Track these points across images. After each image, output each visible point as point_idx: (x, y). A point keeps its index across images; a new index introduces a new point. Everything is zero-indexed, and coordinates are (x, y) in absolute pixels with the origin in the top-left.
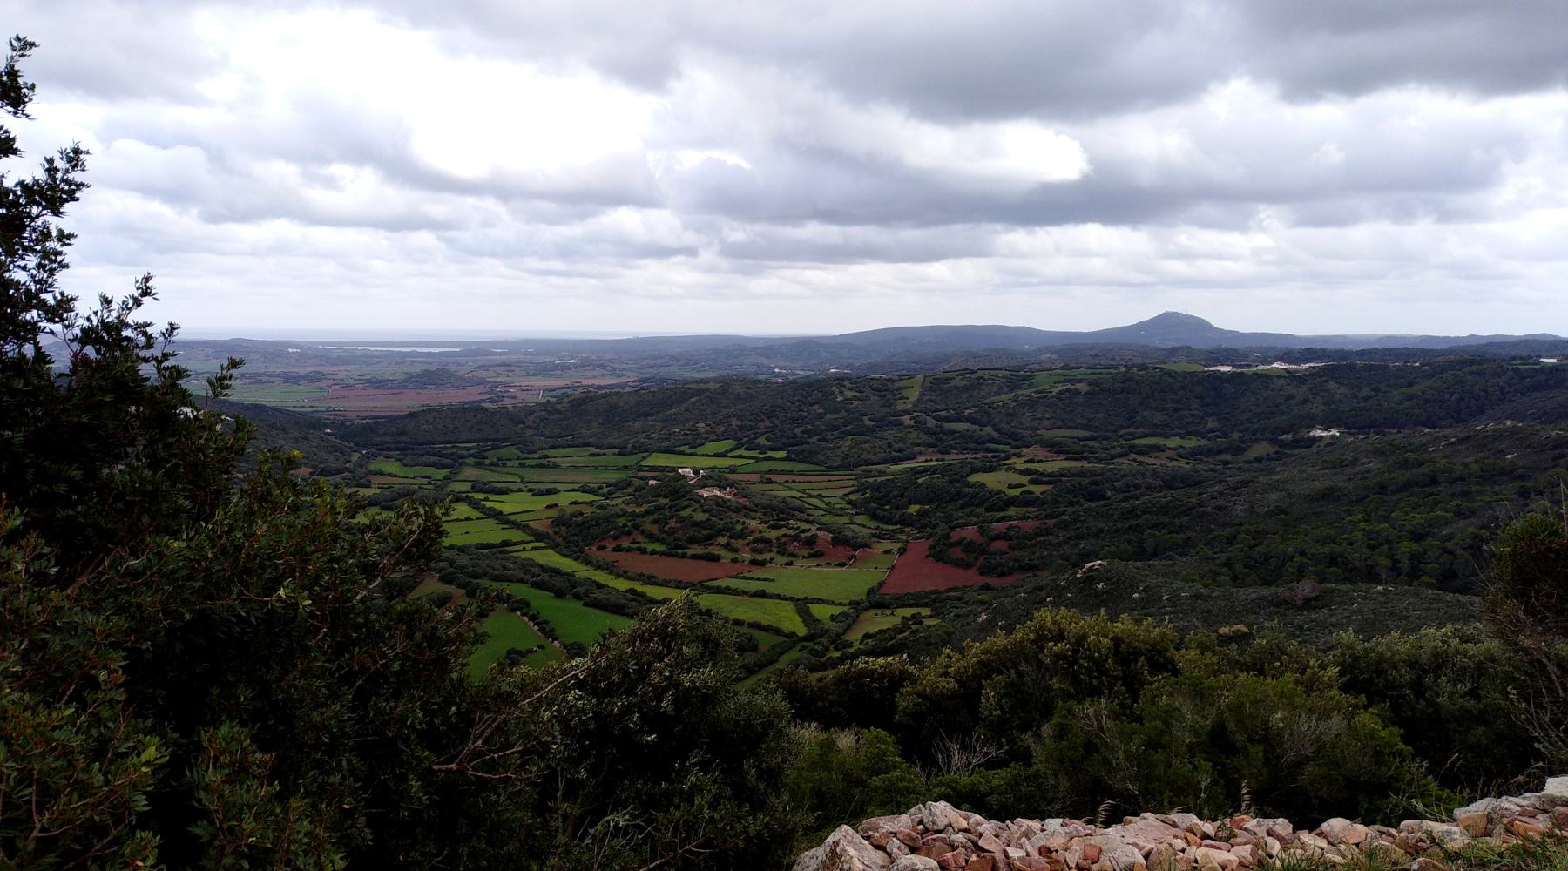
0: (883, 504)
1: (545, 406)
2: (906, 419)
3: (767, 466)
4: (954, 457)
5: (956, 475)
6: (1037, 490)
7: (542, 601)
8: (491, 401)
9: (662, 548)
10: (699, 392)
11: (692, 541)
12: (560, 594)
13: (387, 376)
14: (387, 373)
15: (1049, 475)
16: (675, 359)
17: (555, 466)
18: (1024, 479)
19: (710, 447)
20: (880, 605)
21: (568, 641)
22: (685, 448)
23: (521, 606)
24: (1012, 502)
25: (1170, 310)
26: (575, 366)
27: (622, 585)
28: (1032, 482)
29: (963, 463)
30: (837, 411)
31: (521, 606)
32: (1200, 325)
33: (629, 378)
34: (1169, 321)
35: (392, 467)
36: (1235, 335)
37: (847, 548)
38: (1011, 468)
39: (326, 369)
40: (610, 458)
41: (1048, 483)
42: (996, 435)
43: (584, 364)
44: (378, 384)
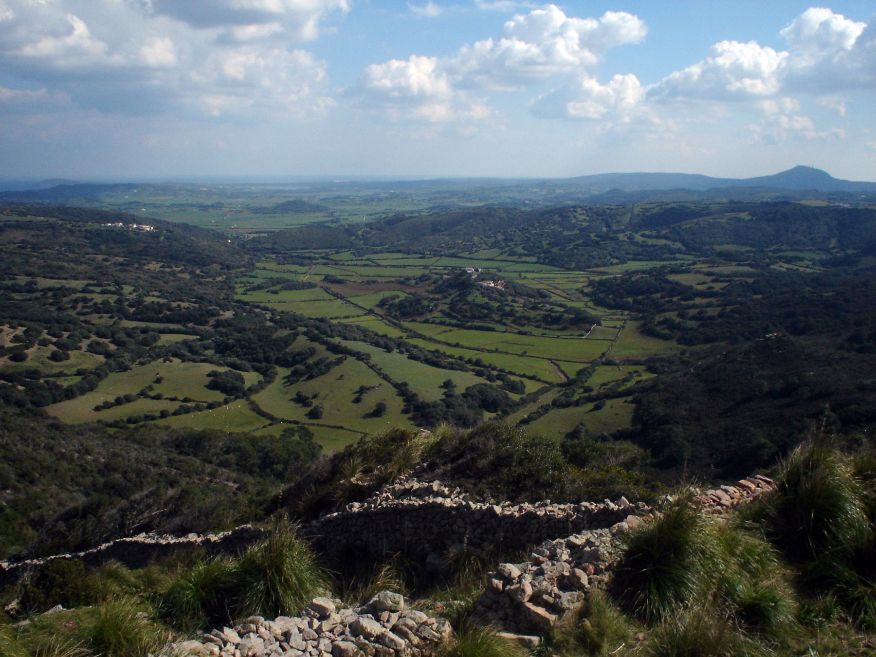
0: (607, 294)
1: (370, 225)
2: (621, 237)
3: (521, 267)
4: (658, 264)
5: (658, 274)
6: (718, 287)
7: (378, 355)
8: (332, 222)
9: (454, 321)
10: (476, 214)
11: (473, 318)
12: (389, 350)
13: (264, 205)
14: (265, 203)
15: (727, 276)
16: (453, 194)
17: (343, 265)
18: (708, 279)
19: (483, 254)
20: (610, 363)
21: (182, 399)
22: (465, 254)
23: (359, 356)
24: (701, 294)
25: (802, 164)
26: (387, 199)
27: (432, 347)
28: (714, 281)
29: (664, 267)
30: (571, 230)
31: (359, 356)
32: (822, 176)
33: (424, 206)
34: (801, 172)
35: (272, 265)
36: (846, 182)
37: (580, 322)
38: (698, 272)
39: (224, 201)
40: (414, 260)
41: (723, 281)
42: (683, 248)
43: (392, 197)
44: (258, 211)
